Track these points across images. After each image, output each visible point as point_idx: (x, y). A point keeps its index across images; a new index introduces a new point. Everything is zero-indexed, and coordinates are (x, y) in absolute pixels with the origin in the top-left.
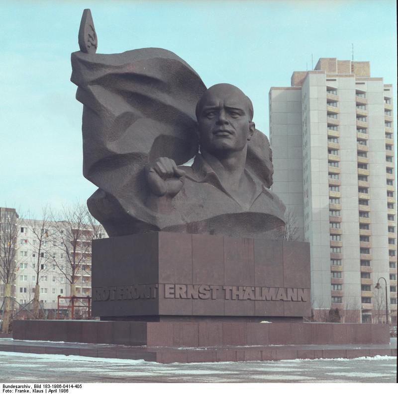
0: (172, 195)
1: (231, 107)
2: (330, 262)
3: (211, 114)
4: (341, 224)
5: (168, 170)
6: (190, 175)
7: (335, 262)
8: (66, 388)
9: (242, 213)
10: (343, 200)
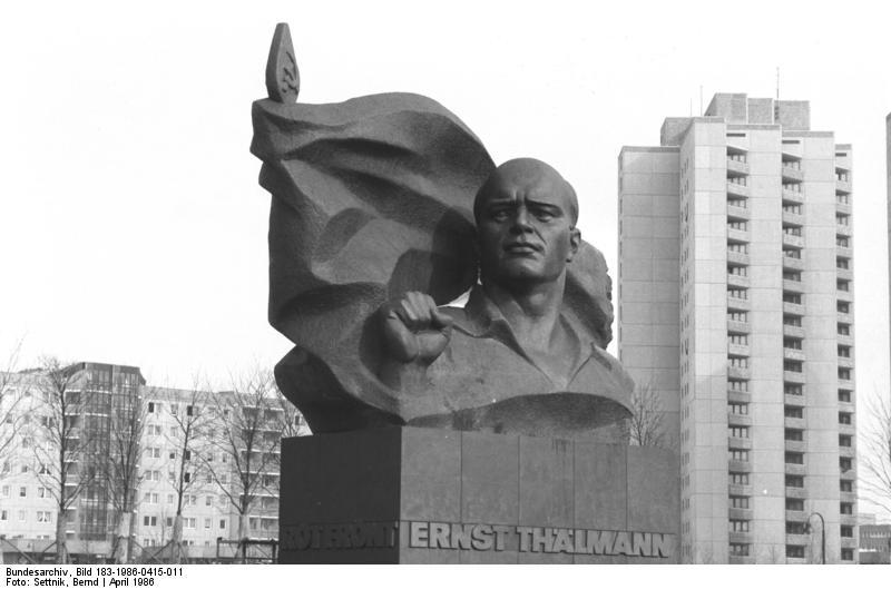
0: (427, 360)
1: (538, 200)
2: (726, 478)
3: (503, 213)
4: (750, 405)
5: (421, 315)
6: (462, 324)
7: (738, 477)
8: (148, 576)
9: (553, 395)
10: (754, 361)
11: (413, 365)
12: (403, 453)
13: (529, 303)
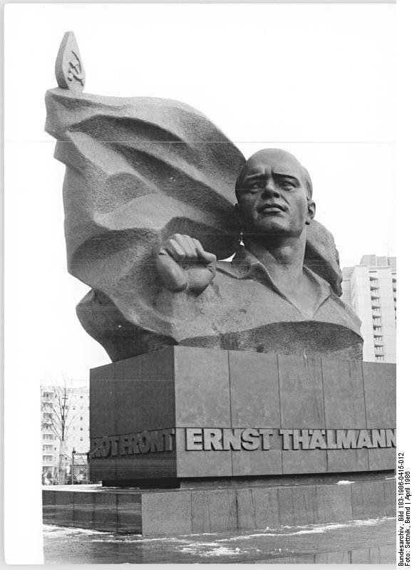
1: (281, 173)
3: (255, 186)
11: (183, 294)
12: (176, 369)
13: (280, 254)
